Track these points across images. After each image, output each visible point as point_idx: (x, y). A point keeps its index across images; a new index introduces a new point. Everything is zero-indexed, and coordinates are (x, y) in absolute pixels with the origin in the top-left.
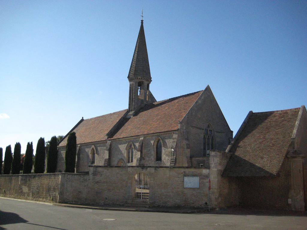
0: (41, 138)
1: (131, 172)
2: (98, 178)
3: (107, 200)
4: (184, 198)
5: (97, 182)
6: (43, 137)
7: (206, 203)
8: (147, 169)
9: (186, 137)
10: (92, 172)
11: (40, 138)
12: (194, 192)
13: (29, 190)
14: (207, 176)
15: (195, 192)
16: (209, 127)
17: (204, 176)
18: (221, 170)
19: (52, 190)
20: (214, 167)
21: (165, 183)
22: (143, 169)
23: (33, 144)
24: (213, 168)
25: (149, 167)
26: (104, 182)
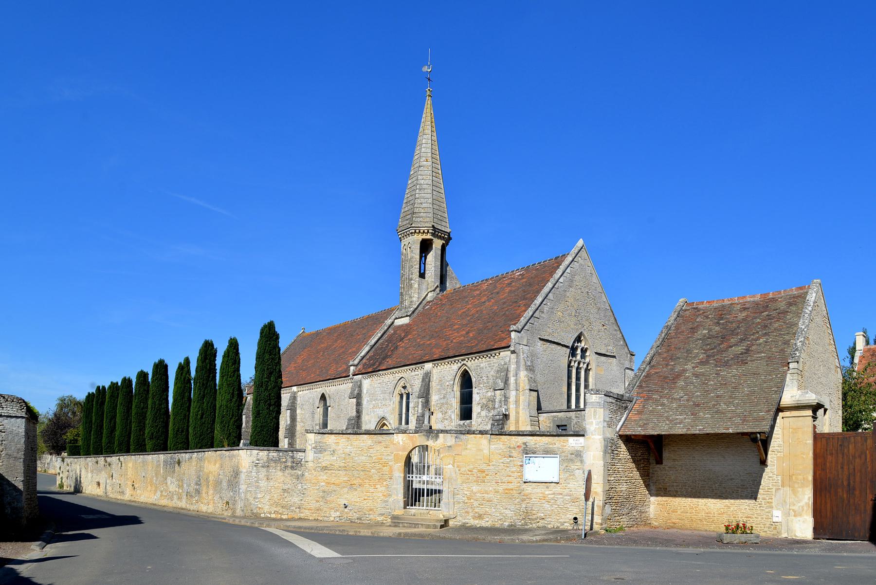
0: (142, 371)
1: (401, 443)
2: (326, 459)
3: (346, 510)
4: (524, 506)
5: (325, 468)
6: (104, 385)
7: (575, 519)
8: (437, 437)
9: (529, 363)
10: (313, 445)
11: (87, 394)
12: (547, 493)
13: (180, 487)
14: (578, 455)
15: (550, 492)
16: (578, 339)
17: (572, 454)
18: (506, 425)
19: (225, 484)
20: (595, 431)
21: (479, 471)
22: (428, 437)
23: (142, 524)
24: (592, 435)
25: (442, 431)
26: (340, 467)
